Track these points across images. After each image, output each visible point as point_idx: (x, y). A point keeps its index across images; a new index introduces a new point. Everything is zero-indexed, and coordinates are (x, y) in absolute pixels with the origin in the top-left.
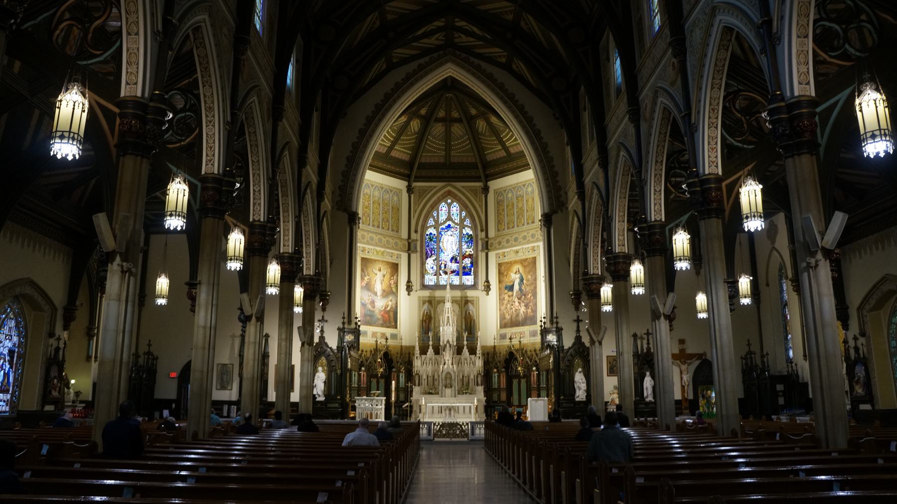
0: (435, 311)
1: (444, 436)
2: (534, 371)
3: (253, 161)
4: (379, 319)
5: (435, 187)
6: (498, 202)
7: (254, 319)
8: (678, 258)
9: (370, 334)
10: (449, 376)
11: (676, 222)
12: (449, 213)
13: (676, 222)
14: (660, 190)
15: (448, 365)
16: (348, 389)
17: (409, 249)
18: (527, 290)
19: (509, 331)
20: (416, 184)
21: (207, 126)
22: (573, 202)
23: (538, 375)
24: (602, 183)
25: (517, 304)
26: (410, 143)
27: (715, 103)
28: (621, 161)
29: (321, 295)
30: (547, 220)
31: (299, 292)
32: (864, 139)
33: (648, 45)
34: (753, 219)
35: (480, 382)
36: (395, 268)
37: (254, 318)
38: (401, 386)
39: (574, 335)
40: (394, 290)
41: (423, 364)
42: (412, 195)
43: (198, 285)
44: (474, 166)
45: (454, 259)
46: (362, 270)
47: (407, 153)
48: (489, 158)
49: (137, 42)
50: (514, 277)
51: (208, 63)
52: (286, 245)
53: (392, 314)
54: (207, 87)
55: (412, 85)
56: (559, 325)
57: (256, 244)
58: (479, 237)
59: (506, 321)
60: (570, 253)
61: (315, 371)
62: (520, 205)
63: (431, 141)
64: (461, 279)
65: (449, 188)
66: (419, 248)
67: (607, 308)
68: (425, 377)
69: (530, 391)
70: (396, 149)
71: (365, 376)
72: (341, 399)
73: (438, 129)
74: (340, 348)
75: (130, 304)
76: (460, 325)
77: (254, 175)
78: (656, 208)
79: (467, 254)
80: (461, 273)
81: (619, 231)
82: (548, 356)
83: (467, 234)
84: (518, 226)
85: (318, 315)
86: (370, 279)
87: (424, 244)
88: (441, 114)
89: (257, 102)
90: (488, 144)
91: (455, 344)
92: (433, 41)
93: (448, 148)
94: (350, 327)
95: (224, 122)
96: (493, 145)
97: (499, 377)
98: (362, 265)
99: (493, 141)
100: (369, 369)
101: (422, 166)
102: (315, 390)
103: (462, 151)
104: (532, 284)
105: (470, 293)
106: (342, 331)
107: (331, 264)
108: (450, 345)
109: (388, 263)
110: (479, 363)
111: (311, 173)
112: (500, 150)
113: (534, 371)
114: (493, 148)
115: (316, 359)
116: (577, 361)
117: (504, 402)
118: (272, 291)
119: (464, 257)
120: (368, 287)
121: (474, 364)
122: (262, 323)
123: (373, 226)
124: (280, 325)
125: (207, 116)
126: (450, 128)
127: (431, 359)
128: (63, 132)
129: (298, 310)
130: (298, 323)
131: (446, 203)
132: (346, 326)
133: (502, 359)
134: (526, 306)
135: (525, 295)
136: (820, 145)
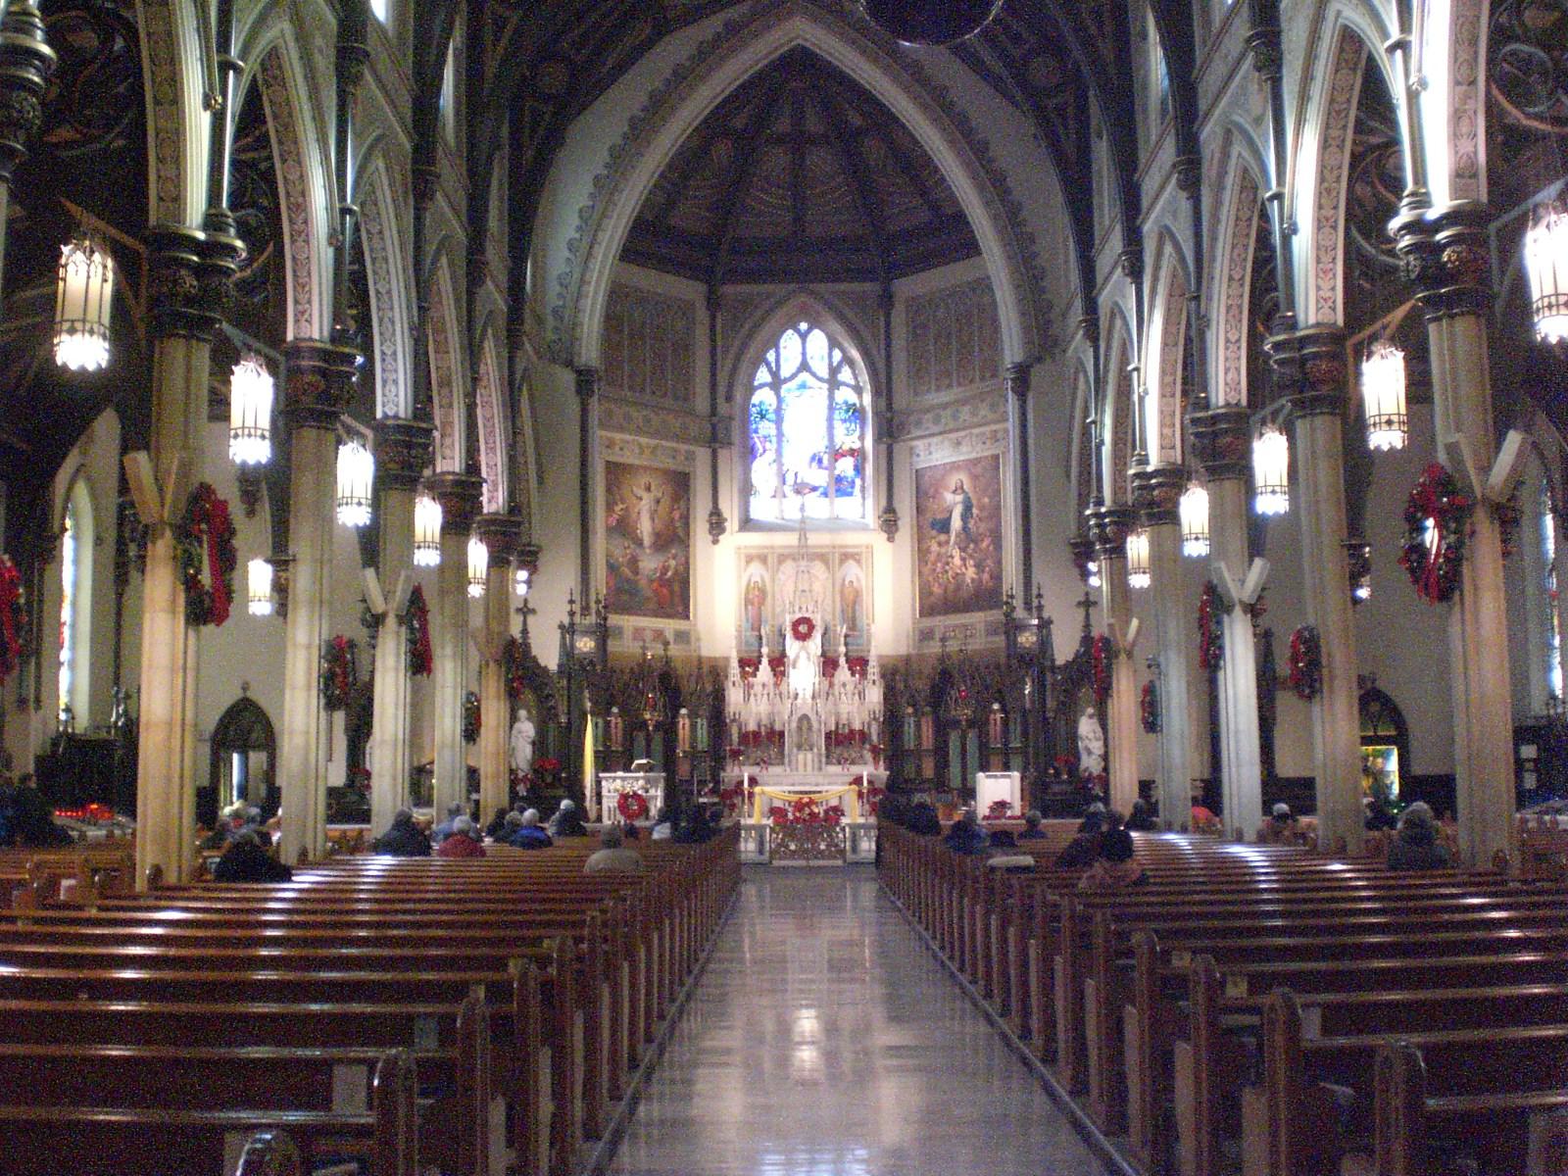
2: (995, 712)
8: (1270, 489)
9: (628, 633)
18: (981, 530)
20: (729, 290)
23: (1005, 722)
25: (957, 561)
32: (1538, 309)
34: (1547, 313)
38: (700, 748)
40: (681, 534)
43: (291, 565)
46: (609, 490)
52: (450, 461)
53: (676, 588)
56: (1046, 615)
59: (932, 599)
69: (987, 756)
71: (620, 725)
77: (381, 320)
78: (1230, 376)
86: (627, 509)
97: (918, 726)
109: (666, 472)
110: (875, 695)
113: (995, 712)
117: (928, 780)
119: (837, 455)
121: (862, 695)
123: (631, 388)
128: (73, 321)
131: (798, 331)
134: (979, 566)
135: (976, 543)
136: (1494, 297)
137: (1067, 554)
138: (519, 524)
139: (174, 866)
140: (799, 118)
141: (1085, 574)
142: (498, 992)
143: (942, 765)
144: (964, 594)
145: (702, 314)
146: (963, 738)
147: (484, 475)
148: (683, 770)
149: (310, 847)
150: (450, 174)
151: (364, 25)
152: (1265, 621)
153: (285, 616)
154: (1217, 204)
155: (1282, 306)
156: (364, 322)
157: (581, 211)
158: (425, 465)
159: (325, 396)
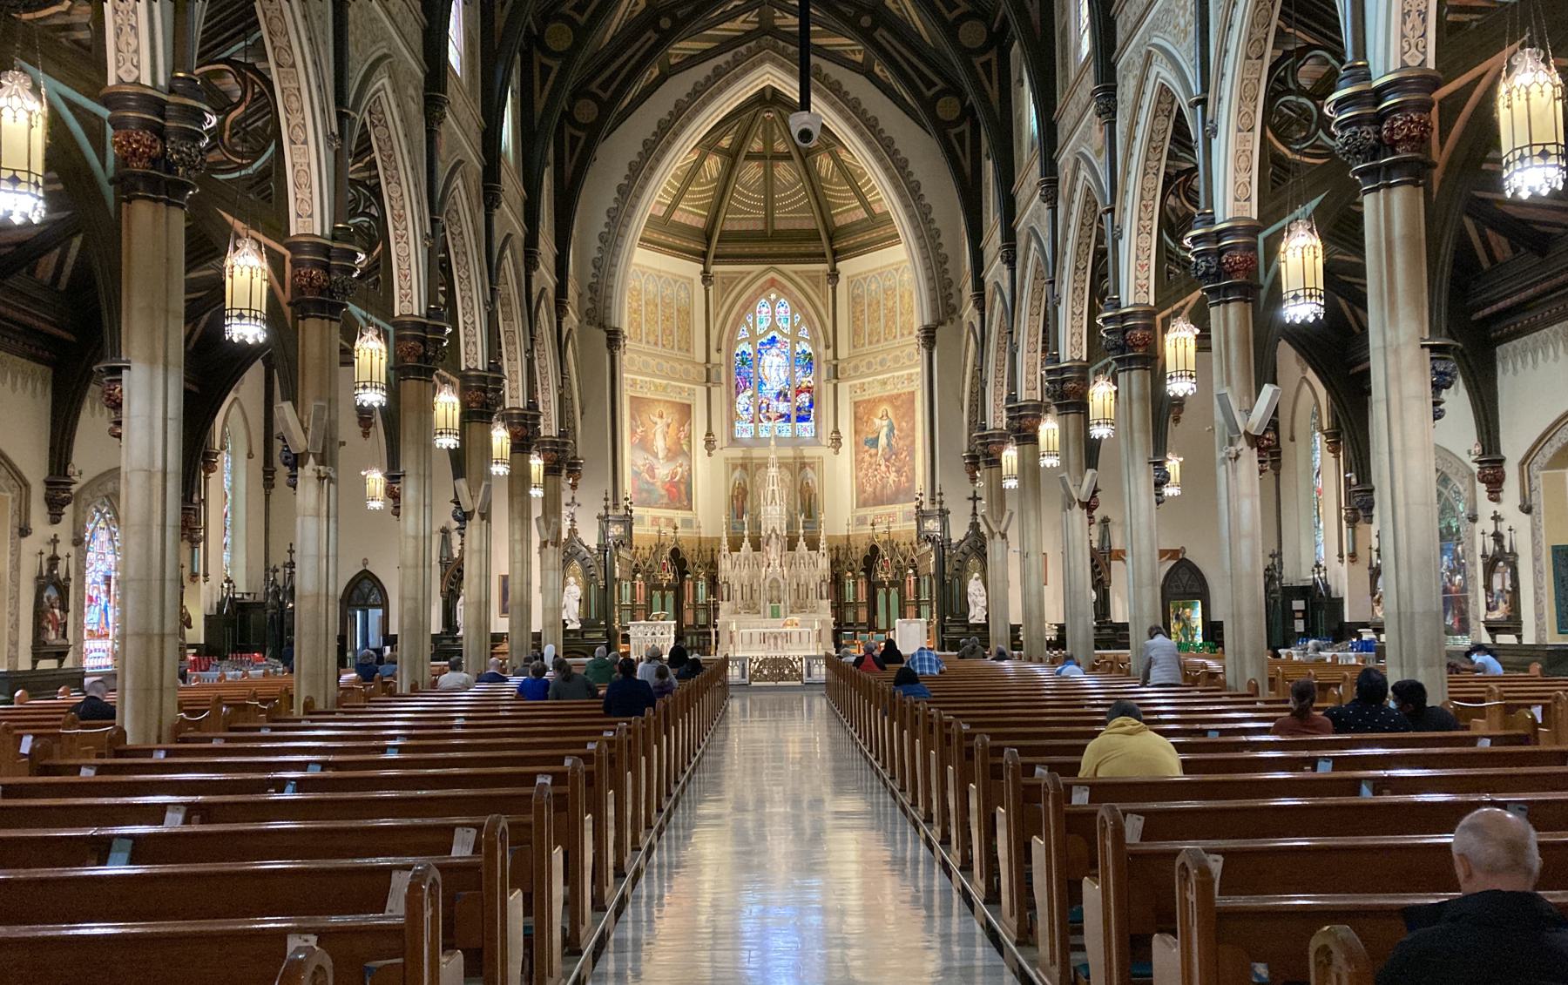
0: (752, 483)
1: (766, 678)
3: (459, 276)
4: (662, 496)
5: (749, 273)
6: (853, 299)
7: (476, 516)
10: (775, 584)
11: (1176, 306)
12: (773, 316)
13: (1176, 306)
14: (1082, 313)
15: (775, 567)
16: (616, 609)
17: (708, 380)
19: (870, 512)
21: (397, 243)
22: (969, 312)
23: (918, 581)
24: (1006, 285)
25: (883, 468)
26: (705, 198)
27: (1148, 196)
28: (1031, 258)
29: (569, 465)
30: (929, 337)
31: (536, 464)
32: (1508, 163)
33: (1072, 77)
35: (825, 594)
36: (686, 411)
37: (476, 515)
39: (969, 520)
40: (685, 448)
41: (734, 566)
42: (711, 288)
44: (813, 236)
45: (781, 395)
46: (633, 417)
47: (702, 216)
48: (840, 221)
49: (306, 154)
50: (880, 424)
51: (392, 148)
52: (514, 396)
53: (682, 487)
54: (393, 184)
55: (704, 104)
56: (944, 507)
57: (474, 405)
58: (823, 358)
60: (963, 391)
61: (565, 584)
62: (890, 304)
63: (739, 193)
64: (794, 428)
65: (772, 274)
66: (724, 379)
67: (1011, 484)
68: (737, 587)
69: (905, 606)
70: (682, 209)
72: (606, 626)
73: (751, 172)
74: (602, 548)
75: (332, 520)
76: (792, 503)
77: (463, 298)
79: (804, 385)
80: (793, 418)
81: (1028, 368)
82: (928, 553)
83: (804, 352)
84: (886, 339)
85: (566, 497)
87: (733, 369)
88: (756, 145)
89: (461, 188)
90: (840, 198)
91: (785, 533)
92: (737, 25)
93: (769, 206)
94: (617, 513)
95: (422, 236)
96: (845, 198)
97: (855, 584)
98: (631, 408)
99: (847, 191)
100: (648, 577)
101: (726, 237)
102: (564, 612)
103: (793, 212)
104: (908, 436)
105: (809, 452)
106: (604, 520)
107: (582, 413)
108: (777, 536)
109: (673, 404)
110: (824, 564)
111: (545, 276)
112: (856, 208)
114: (845, 205)
115: (566, 562)
116: (973, 562)
118: (500, 470)
119: (799, 392)
120: (644, 444)
121: (815, 564)
122: (489, 521)
123: (648, 342)
124: (511, 520)
125: (396, 228)
126: (772, 170)
127: (747, 558)
129: (537, 493)
130: (537, 512)
131: (768, 299)
132: (610, 512)
133: (860, 557)
137: (962, 464)
138: (565, 444)
139: (322, 698)
140: (768, 141)
141: (973, 479)
142: (559, 778)
143: (873, 611)
144: (888, 491)
145: (699, 287)
146: (888, 594)
147: (541, 409)
148: (689, 618)
149: (419, 680)
150: (511, 186)
151: (445, 72)
152: (1098, 514)
153: (398, 515)
154: (1068, 213)
155: (1111, 291)
156: (450, 294)
157: (608, 211)
158: (497, 404)
159: (424, 358)
